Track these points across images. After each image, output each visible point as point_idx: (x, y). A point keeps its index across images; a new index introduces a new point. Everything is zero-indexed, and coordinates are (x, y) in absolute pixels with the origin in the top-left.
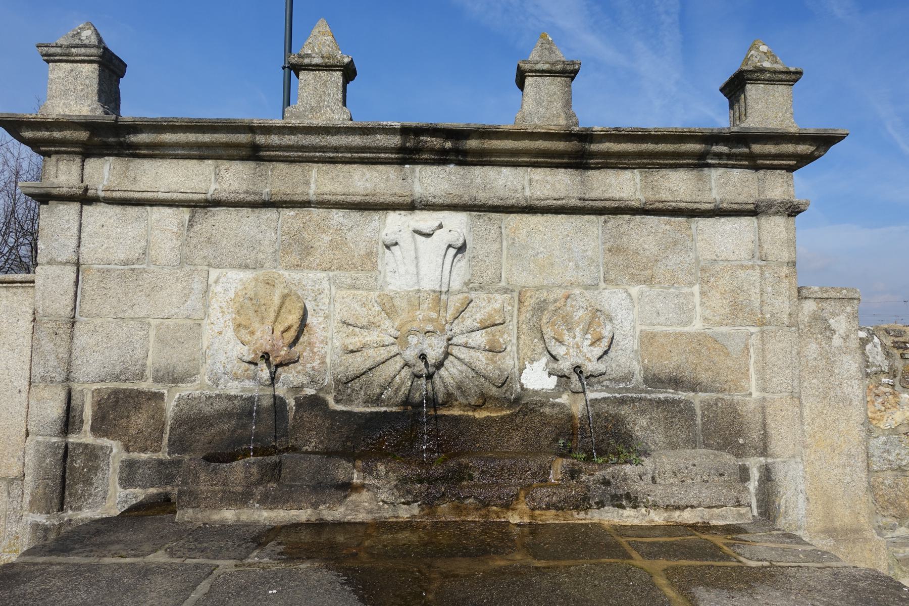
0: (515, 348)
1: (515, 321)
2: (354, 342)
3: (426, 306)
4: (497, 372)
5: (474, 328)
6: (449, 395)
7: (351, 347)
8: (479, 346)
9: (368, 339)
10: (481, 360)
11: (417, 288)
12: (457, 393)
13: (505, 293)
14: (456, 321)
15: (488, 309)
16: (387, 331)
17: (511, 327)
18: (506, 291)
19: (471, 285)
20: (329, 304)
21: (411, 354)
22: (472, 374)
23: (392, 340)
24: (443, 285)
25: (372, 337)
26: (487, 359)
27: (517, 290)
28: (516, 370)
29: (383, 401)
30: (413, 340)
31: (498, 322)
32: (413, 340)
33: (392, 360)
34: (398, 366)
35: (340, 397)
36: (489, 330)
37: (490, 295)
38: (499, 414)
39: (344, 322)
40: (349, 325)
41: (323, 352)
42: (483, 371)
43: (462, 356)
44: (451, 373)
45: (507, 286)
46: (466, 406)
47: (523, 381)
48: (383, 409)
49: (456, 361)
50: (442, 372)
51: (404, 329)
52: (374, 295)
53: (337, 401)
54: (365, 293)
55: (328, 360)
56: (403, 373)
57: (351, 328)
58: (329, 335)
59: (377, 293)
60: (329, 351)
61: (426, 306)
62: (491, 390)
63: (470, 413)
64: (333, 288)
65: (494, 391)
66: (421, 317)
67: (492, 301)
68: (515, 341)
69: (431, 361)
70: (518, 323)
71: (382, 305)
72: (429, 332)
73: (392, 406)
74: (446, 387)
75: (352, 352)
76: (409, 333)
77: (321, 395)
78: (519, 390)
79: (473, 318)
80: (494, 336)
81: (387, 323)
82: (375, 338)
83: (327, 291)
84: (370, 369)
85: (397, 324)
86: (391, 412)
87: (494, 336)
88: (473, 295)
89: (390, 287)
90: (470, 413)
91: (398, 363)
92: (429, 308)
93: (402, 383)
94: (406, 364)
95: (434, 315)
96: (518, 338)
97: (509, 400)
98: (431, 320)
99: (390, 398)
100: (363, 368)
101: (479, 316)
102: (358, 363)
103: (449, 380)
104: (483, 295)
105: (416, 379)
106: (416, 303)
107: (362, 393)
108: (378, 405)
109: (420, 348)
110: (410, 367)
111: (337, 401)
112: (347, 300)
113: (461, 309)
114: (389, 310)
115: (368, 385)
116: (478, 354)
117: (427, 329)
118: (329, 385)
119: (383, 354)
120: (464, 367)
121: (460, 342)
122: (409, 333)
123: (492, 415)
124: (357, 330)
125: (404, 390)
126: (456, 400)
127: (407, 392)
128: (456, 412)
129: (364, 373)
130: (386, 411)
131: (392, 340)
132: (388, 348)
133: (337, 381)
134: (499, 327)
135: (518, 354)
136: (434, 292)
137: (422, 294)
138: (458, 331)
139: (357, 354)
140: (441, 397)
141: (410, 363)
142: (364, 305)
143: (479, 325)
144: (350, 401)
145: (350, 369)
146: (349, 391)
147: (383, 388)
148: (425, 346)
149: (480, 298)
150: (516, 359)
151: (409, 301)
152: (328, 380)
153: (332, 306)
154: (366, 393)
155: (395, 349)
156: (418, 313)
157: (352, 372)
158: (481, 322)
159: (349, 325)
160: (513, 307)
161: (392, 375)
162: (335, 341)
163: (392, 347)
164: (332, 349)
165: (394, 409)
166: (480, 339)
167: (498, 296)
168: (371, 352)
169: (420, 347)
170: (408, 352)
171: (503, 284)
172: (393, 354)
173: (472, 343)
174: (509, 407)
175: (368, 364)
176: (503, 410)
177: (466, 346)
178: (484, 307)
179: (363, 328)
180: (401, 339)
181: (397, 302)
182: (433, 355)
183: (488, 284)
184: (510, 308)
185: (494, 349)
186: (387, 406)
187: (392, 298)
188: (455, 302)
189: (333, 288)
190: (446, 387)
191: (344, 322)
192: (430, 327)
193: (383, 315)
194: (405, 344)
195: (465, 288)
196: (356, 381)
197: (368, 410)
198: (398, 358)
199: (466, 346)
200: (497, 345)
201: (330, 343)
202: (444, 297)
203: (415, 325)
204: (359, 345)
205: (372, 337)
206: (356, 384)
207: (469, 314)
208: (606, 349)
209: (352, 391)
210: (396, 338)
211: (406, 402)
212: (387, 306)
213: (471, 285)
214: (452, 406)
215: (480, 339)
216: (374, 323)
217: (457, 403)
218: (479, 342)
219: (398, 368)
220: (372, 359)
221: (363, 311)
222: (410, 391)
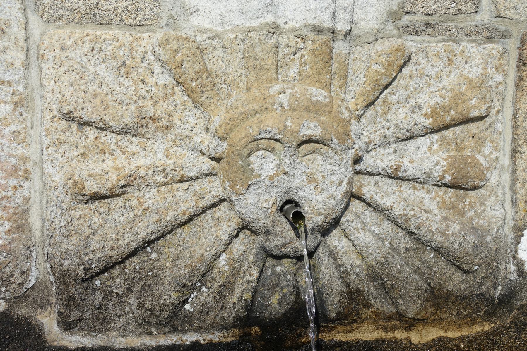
0: (506, 177)
1: (509, 111)
2: (103, 170)
3: (293, 71)
4: (471, 238)
5: (416, 130)
6: (353, 295)
7: (92, 187)
8: (428, 175)
9: (141, 162)
10: (428, 209)
11: (269, 19)
12: (369, 289)
13: (489, 39)
14: (369, 113)
15: (451, 80)
16: (184, 145)
17: (499, 126)
18: (490, 34)
19: (406, 19)
20: (26, 66)
21: (258, 203)
22: (407, 242)
23: (206, 164)
24: (340, 15)
25: (149, 156)
26: (443, 205)
27: (517, 34)
28: (508, 230)
29: (189, 318)
30: (265, 164)
31: (475, 113)
32: (265, 164)
33: (202, 220)
34: (225, 230)
35: (75, 314)
36: (448, 133)
37: (453, 46)
38: (466, 332)
39: (69, 117)
40: (83, 124)
41: (18, 198)
42: (438, 237)
43: (386, 202)
44: (361, 241)
45: (495, 23)
46: (390, 318)
47: (522, 255)
48: (190, 338)
49: (368, 215)
50: (335, 239)
51: (240, 135)
52: (149, 40)
53: (68, 326)
54: (125, 36)
55: (35, 221)
56: (237, 247)
57: (92, 133)
58: (32, 151)
59: (159, 35)
60: (35, 197)
61: (293, 71)
62: (450, 279)
63: (400, 335)
64: (35, 21)
65: (456, 281)
66: (284, 99)
67: (459, 61)
68: (506, 161)
69: (314, 219)
70: (515, 117)
71: (174, 68)
72: (309, 141)
73: (210, 329)
74: (343, 276)
75: (96, 197)
76: (255, 143)
77: (22, 311)
78: (513, 276)
79: (422, 95)
80: (460, 148)
81: (189, 120)
82: (159, 159)
83: (17, 31)
84: (150, 243)
85: (218, 120)
86: (211, 344)
87: (460, 148)
88: (412, 44)
89: (196, 21)
90: (400, 335)
91: (224, 223)
92: (302, 77)
93: (236, 272)
94: (245, 226)
95: (319, 94)
96: (514, 151)
97: (488, 300)
98: (314, 109)
99: (205, 310)
100: (129, 240)
101: (428, 99)
102: (116, 227)
103: (350, 259)
104: (435, 45)
105: (270, 262)
106: (270, 61)
107: (133, 301)
108: (175, 330)
109: (283, 187)
110: (254, 232)
111: (68, 326)
112: (76, 54)
113: (385, 81)
114: (195, 83)
115: (147, 282)
116: (421, 193)
117: (305, 133)
118: (42, 286)
119: (183, 200)
120: (388, 227)
121: (381, 165)
122: (255, 143)
123: (450, 335)
124: (109, 138)
125: (240, 291)
126: (368, 306)
127: (248, 296)
128: (368, 334)
129: (134, 253)
130: (196, 344)
131: (206, 164)
132: (196, 186)
133: (63, 277)
134: (473, 127)
135: (514, 191)
136: (318, 30)
137: (282, 39)
138: (376, 139)
139: (114, 203)
140: (333, 305)
141: (256, 226)
142: (124, 69)
143: (427, 122)
144: (101, 321)
145: (94, 245)
146: (98, 297)
147: (186, 288)
148: (297, 181)
149: (427, 49)
150: (508, 204)
151: (249, 58)
152: (38, 271)
153: (34, 72)
154: (141, 305)
155: (214, 188)
156: (277, 88)
157: (99, 251)
158: (434, 114)
159: (83, 124)
160: (506, 75)
161: (208, 255)
162: (49, 168)
163: (205, 184)
164: (43, 190)
165: (216, 337)
166: (427, 156)
167: (471, 48)
168: (151, 197)
169: (283, 183)
170: (251, 198)
171: (484, 16)
172: (208, 200)
173: (411, 169)
174: (488, 316)
175: (143, 230)
176: (474, 322)
177: (395, 176)
178: (438, 77)
179: (123, 131)
180: (231, 163)
181: (216, 62)
182: (317, 205)
183: (447, 16)
184: (499, 78)
185: (461, 183)
186: (199, 330)
187: (202, 51)
188: (363, 65)
189: (35, 21)
190: (343, 276)
191: (69, 117)
192: (312, 129)
193: (180, 96)
194: (245, 178)
195: (390, 26)
196: (116, 271)
197: (151, 342)
198: (223, 210)
199: (395, 176)
200: (472, 172)
201: (36, 176)
202: (340, 47)
203: (271, 123)
204: (114, 179)
205: (149, 156)
206: (117, 281)
207: (401, 94)
208: (103, 192)
209: (108, 296)
210: (218, 160)
211: (249, 317)
212: (190, 69)
213: (406, 19)
214: (358, 320)
215: (427, 156)
216: (155, 119)
217: (369, 312)
218: (427, 165)
219: (225, 238)
220: (152, 217)
221: (125, 87)
222: (255, 291)
